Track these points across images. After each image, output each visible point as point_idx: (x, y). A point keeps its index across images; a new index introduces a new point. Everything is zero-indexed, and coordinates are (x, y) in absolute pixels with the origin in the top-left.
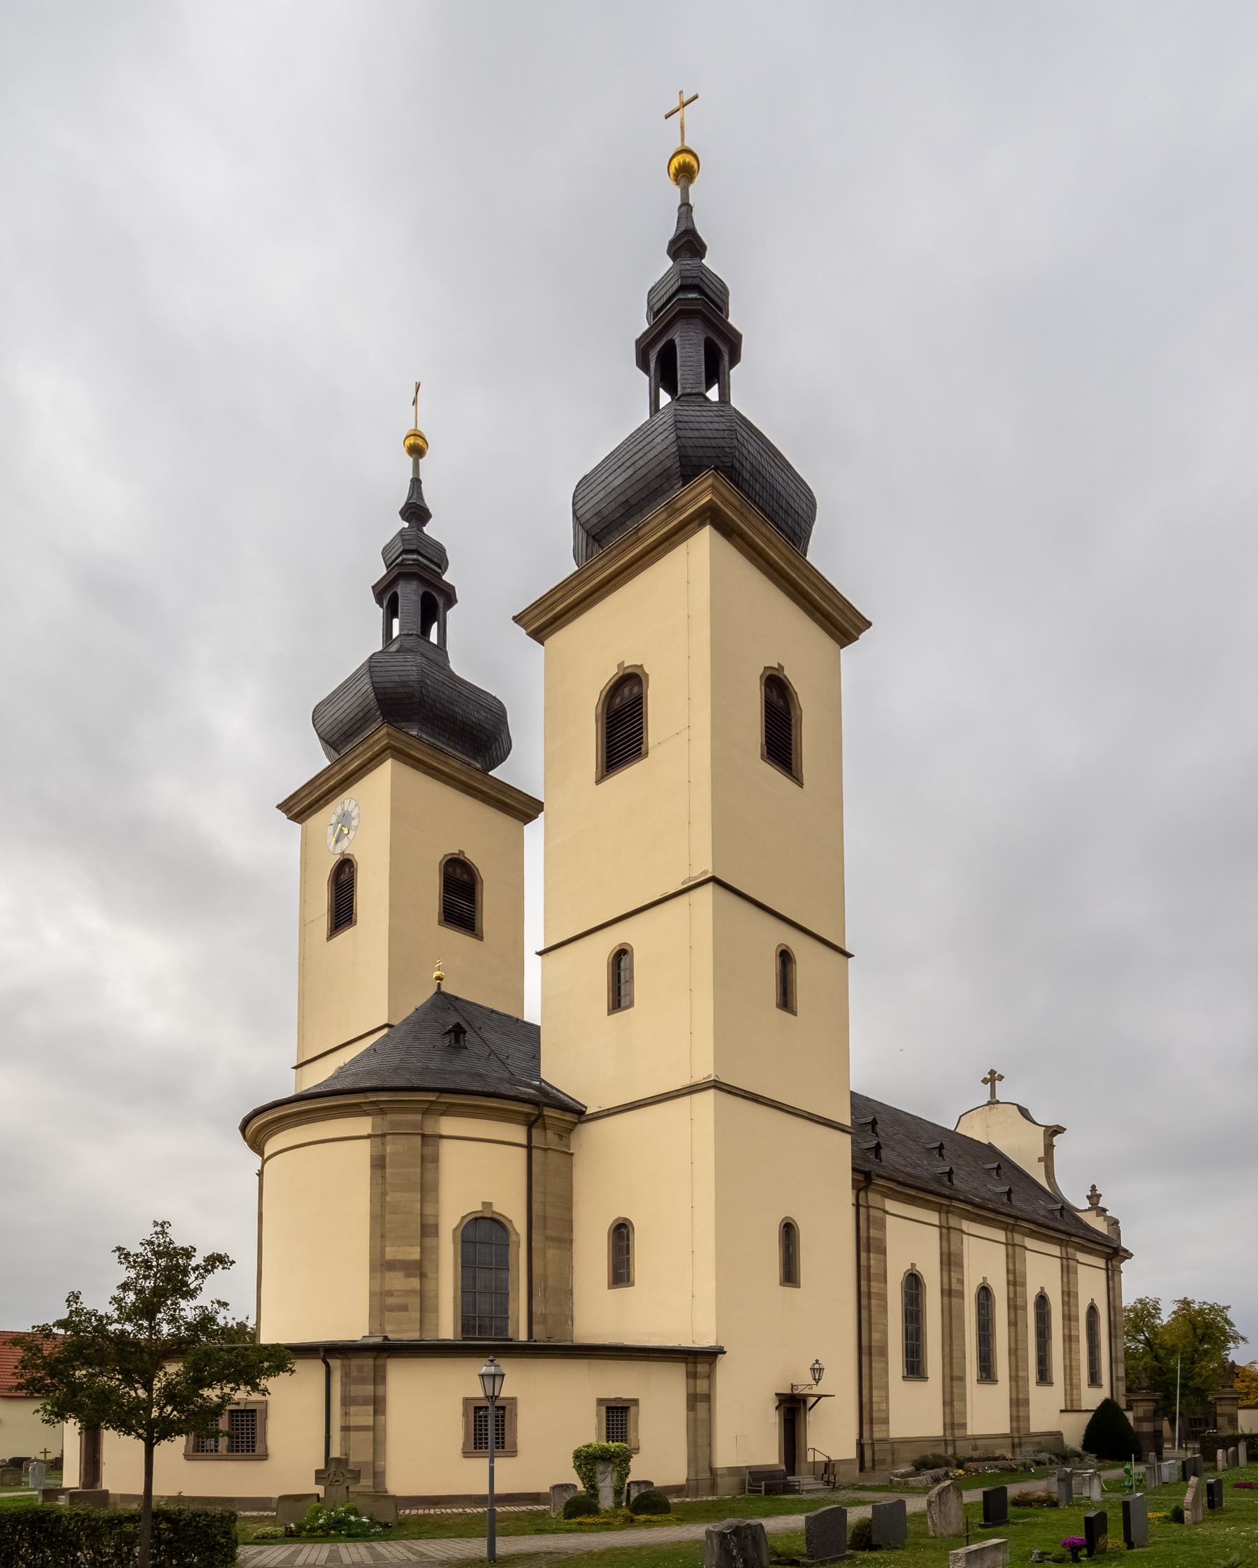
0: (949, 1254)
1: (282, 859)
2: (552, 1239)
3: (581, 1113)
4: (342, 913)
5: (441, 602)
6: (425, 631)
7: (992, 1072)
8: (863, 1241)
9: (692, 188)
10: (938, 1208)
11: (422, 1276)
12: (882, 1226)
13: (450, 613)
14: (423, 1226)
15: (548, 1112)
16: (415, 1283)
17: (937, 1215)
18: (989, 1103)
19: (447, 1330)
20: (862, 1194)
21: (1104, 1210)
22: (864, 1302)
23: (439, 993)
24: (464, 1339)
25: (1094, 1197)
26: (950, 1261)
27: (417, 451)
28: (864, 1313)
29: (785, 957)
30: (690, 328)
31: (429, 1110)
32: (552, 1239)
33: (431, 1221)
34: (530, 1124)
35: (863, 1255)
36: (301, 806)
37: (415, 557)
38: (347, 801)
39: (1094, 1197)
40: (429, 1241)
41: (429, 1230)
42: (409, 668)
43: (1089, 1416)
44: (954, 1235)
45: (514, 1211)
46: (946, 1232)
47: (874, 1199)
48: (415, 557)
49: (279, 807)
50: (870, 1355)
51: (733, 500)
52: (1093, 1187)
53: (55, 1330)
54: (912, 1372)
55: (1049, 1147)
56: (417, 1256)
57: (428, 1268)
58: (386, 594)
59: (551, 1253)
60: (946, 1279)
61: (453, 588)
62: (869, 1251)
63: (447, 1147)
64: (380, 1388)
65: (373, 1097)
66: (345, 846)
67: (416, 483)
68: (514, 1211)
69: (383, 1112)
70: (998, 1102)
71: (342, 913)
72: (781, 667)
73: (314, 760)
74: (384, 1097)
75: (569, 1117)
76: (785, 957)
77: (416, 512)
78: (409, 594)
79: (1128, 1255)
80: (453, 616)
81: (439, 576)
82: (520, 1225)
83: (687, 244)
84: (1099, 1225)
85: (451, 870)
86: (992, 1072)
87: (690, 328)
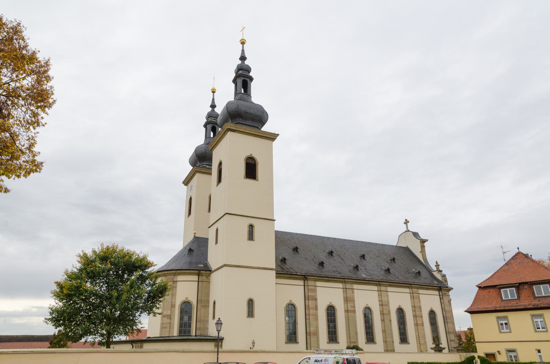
0: (347, 298)
2: (203, 306)
3: (211, 271)
7: (406, 220)
8: (307, 297)
10: (342, 282)
11: (171, 319)
12: (315, 291)
14: (172, 305)
15: (202, 272)
16: (169, 321)
17: (341, 284)
18: (406, 231)
19: (175, 332)
20: (306, 281)
21: (441, 271)
22: (307, 317)
23: (195, 237)
24: (179, 336)
25: (437, 266)
26: (348, 300)
27: (243, 43)
28: (308, 321)
29: (251, 227)
31: (175, 275)
32: (203, 306)
33: (173, 304)
34: (199, 275)
35: (307, 302)
39: (437, 266)
40: (173, 309)
41: (173, 306)
43: (538, 360)
44: (349, 292)
45: (193, 300)
46: (345, 289)
47: (311, 283)
50: (310, 335)
51: (25, 320)
52: (437, 263)
54: (333, 340)
55: (423, 247)
56: (169, 313)
57: (172, 316)
59: (202, 310)
60: (346, 306)
63: (179, 284)
65: (164, 273)
67: (243, 51)
68: (193, 300)
69: (166, 276)
70: (409, 231)
72: (251, 154)
74: (165, 272)
75: (208, 272)
77: (243, 58)
79: (450, 289)
82: (194, 303)
84: (439, 276)
86: (406, 220)
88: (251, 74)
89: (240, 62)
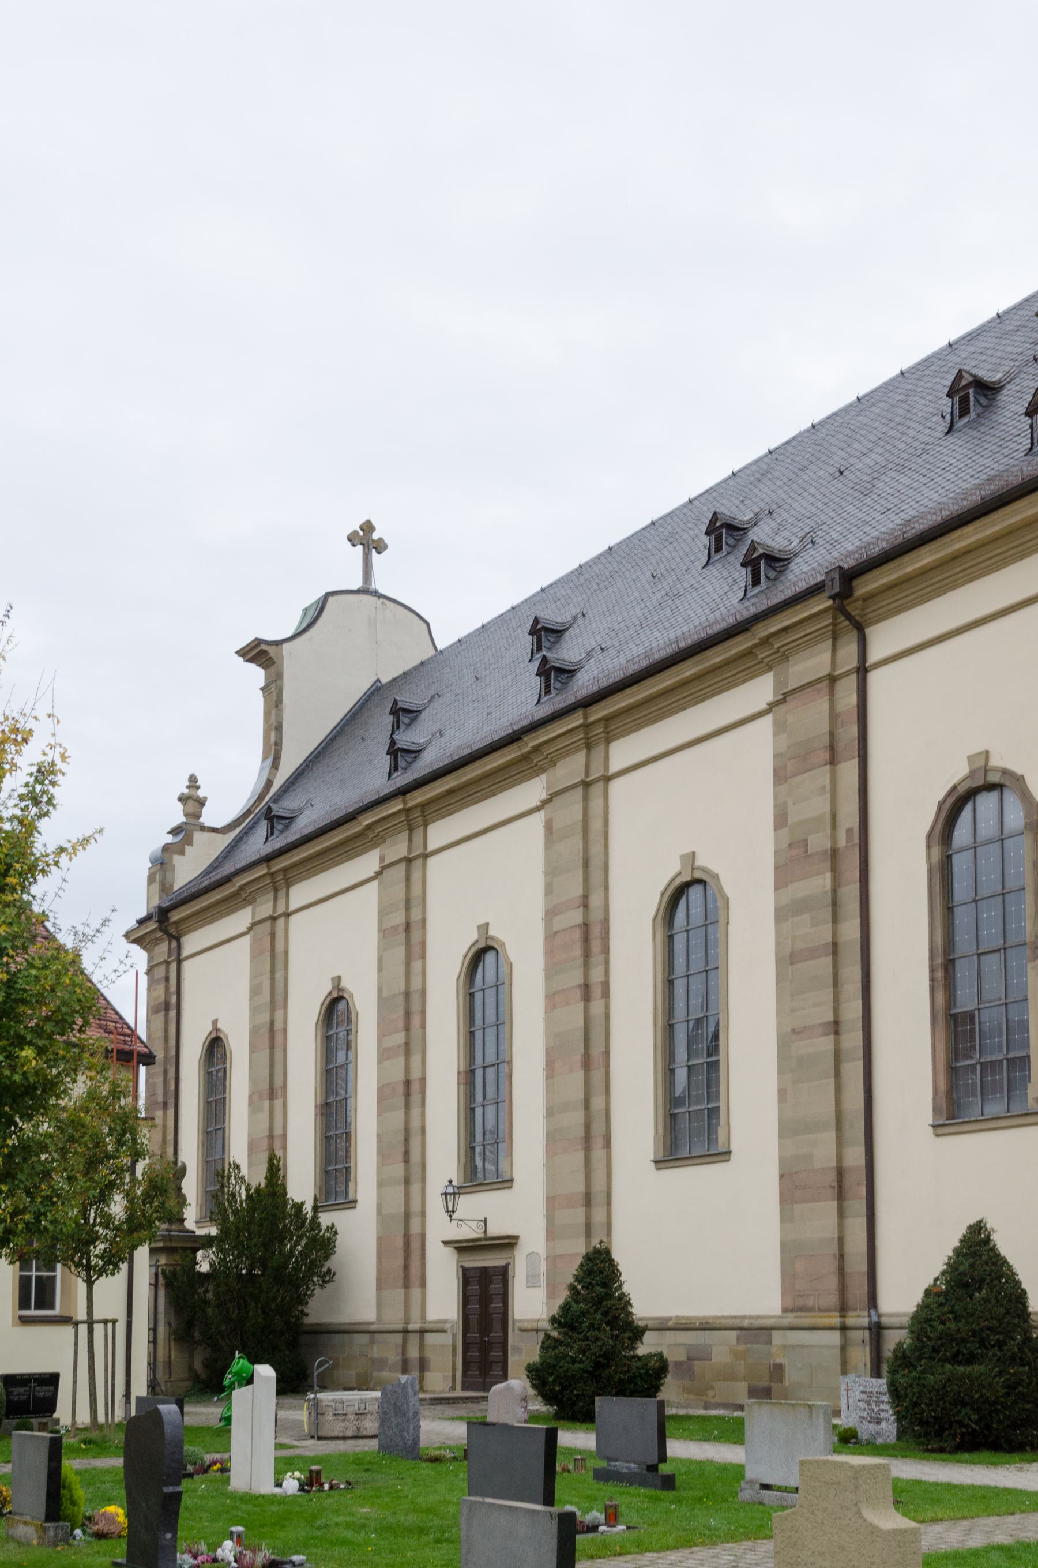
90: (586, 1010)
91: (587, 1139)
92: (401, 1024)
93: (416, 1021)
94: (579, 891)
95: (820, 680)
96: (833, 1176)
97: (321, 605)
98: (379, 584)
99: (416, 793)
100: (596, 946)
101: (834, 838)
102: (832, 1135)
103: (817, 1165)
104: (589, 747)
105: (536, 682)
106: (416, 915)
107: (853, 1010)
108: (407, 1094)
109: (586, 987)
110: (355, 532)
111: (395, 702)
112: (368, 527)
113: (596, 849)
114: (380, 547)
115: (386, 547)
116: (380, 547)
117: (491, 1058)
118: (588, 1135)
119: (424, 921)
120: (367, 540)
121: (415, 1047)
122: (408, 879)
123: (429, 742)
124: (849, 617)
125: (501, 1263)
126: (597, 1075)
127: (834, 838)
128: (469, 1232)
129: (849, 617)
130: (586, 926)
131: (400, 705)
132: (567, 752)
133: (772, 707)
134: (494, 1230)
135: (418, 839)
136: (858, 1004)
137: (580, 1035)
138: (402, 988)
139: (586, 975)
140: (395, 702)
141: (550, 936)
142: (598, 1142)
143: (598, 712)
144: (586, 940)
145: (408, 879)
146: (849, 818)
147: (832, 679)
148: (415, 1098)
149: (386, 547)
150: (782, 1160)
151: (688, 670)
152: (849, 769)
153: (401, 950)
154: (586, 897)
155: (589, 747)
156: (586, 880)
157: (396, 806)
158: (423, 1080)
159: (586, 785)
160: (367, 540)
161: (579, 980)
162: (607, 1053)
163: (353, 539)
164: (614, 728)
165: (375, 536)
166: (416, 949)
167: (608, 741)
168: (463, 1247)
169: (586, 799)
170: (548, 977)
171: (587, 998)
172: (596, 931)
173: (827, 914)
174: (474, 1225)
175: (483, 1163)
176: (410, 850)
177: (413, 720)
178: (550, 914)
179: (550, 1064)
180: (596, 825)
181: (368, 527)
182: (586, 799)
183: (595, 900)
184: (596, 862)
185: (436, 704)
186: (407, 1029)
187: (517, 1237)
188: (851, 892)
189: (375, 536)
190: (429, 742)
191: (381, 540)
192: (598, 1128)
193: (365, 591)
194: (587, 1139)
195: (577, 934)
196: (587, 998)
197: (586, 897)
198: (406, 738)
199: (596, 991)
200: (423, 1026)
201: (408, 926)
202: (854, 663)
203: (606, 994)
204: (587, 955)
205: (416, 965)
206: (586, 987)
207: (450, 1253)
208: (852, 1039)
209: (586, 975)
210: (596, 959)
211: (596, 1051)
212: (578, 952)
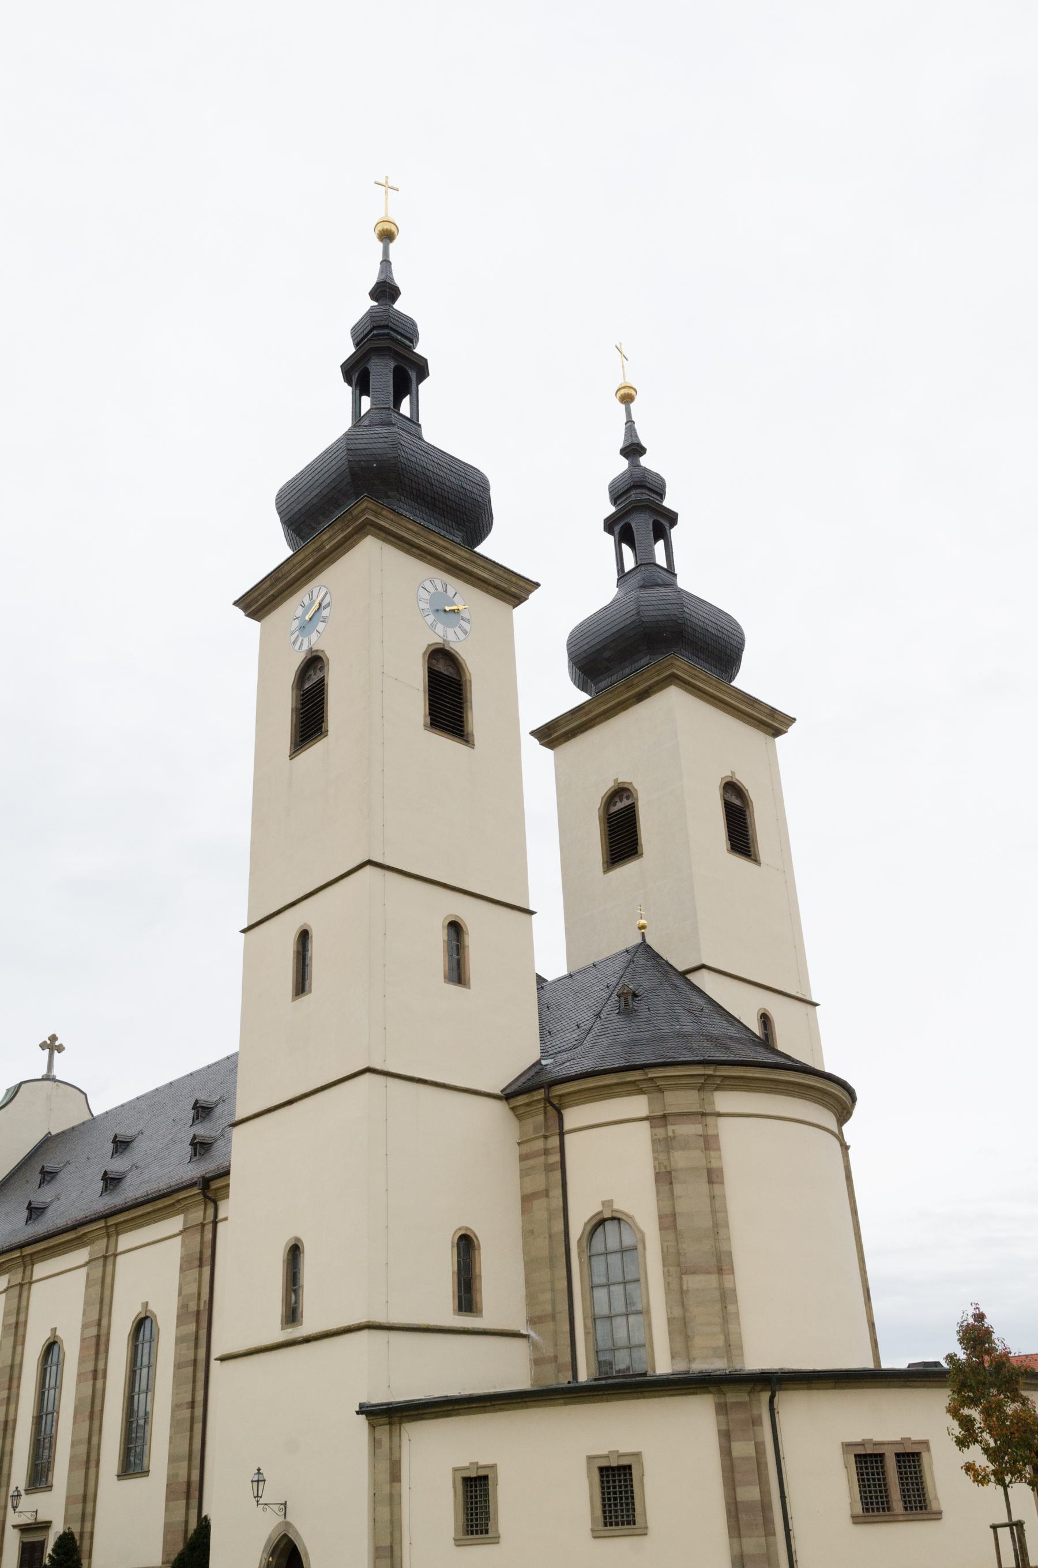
1: (238, 672)
4: (310, 719)
5: (413, 375)
6: (397, 403)
9: (392, 246)
13: (423, 387)
27: (627, 399)
29: (455, 928)
30: (386, 355)
36: (258, 602)
37: (386, 331)
38: (317, 589)
42: (377, 439)
48: (386, 331)
49: (236, 603)
53: (544, 1062)
58: (356, 373)
61: (426, 360)
62: (198, 1312)
64: (727, 1278)
66: (315, 641)
71: (310, 719)
73: (275, 549)
76: (455, 928)
77: (633, 450)
78: (382, 372)
80: (424, 388)
81: (410, 349)
83: (385, 291)
85: (434, 662)
87: (386, 355)
88: (667, 503)
89: (623, 464)
90: (94, 1385)
91: (88, 1462)
92: (6, 1386)
93: (15, 1383)
94: (96, 1317)
95: (197, 1225)
96: (185, 1487)
97: (18, 1088)
98: (58, 1073)
99: (27, 1248)
100: (102, 1348)
101: (198, 1305)
102: (186, 1463)
103: (180, 1480)
104: (108, 1236)
105: (101, 1184)
106: (22, 1318)
107: (200, 1397)
108: (5, 1430)
109: (95, 1371)
110: (45, 1042)
111: (43, 1167)
112: (53, 1038)
113: (107, 1293)
114: (60, 1049)
115: (64, 1049)
116: (60, 1049)
117: (50, 1409)
118: (88, 1461)
119: (26, 1322)
120: (52, 1046)
121: (13, 1400)
122: (20, 1296)
123: (51, 1202)
124: (210, 1198)
125: (42, 1539)
126: (96, 1423)
127: (198, 1305)
128: (26, 1519)
129: (210, 1198)
130: (98, 1336)
131: (46, 1169)
132: (98, 1238)
133: (181, 1233)
134: (41, 1518)
135: (28, 1273)
136: (202, 1392)
137: (89, 1400)
138: (10, 1363)
139: (96, 1365)
140: (43, 1167)
141: (83, 1340)
142: (93, 1464)
143: (111, 1221)
144: (98, 1345)
145: (20, 1296)
146: (205, 1297)
147: (203, 1225)
148: (9, 1432)
149: (64, 1049)
150: (168, 1476)
151: (149, 1208)
152: (207, 1270)
153: (12, 1338)
154: (100, 1320)
155: (108, 1236)
156: (101, 1310)
157: (16, 1254)
158: (15, 1421)
159: (105, 1257)
160: (52, 1046)
161: (92, 1368)
162: (102, 1411)
163: (43, 1046)
164: (120, 1229)
165: (57, 1043)
166: (20, 1339)
167: (118, 1234)
168: (24, 1529)
169: (105, 1265)
170: (79, 1364)
171: (95, 1378)
172: (103, 1339)
173: (192, 1344)
174: (29, 1515)
175: (39, 1476)
176: (23, 1279)
177: (52, 1178)
178: (85, 1326)
179: (75, 1417)
180: (108, 1280)
181: (53, 1038)
182: (105, 1265)
183: (104, 1322)
184: (106, 1301)
185: (69, 1168)
186: (10, 1388)
187: (50, 1522)
188: (203, 1333)
189: (57, 1043)
190: (51, 1202)
191: (61, 1045)
192: (93, 1457)
193: (48, 1078)
194: (88, 1462)
195: (93, 1341)
196: (95, 1378)
197: (100, 1320)
198: (44, 1196)
199: (100, 1375)
200: (18, 1387)
201: (17, 1324)
202: (212, 1218)
203: (105, 1377)
204: (97, 1354)
205: (19, 1349)
206: (95, 1371)
207: (16, 1532)
208: (199, 1411)
209: (96, 1365)
210: (102, 1356)
211: (97, 1409)
212: (93, 1351)
